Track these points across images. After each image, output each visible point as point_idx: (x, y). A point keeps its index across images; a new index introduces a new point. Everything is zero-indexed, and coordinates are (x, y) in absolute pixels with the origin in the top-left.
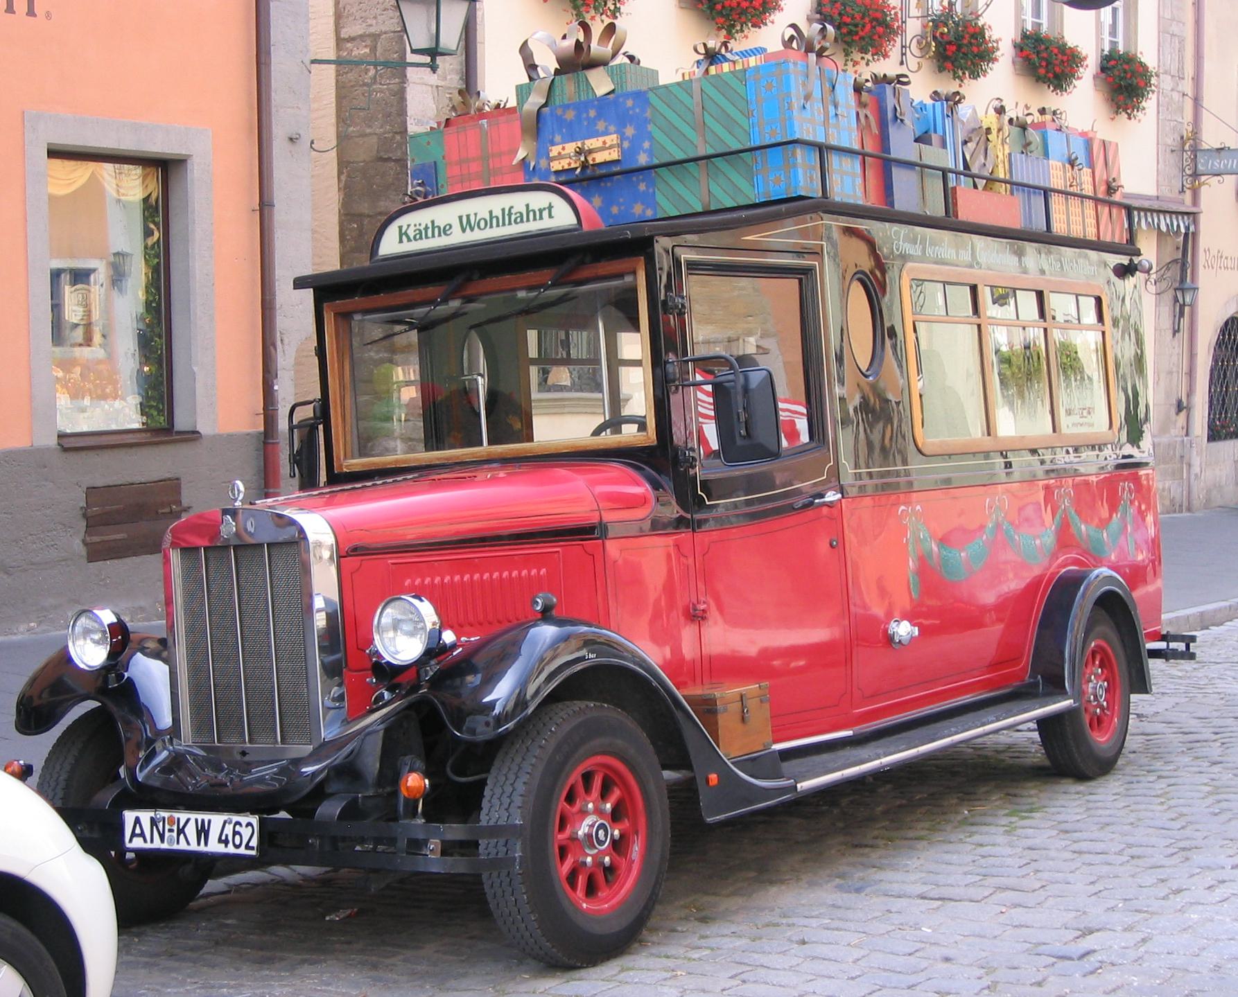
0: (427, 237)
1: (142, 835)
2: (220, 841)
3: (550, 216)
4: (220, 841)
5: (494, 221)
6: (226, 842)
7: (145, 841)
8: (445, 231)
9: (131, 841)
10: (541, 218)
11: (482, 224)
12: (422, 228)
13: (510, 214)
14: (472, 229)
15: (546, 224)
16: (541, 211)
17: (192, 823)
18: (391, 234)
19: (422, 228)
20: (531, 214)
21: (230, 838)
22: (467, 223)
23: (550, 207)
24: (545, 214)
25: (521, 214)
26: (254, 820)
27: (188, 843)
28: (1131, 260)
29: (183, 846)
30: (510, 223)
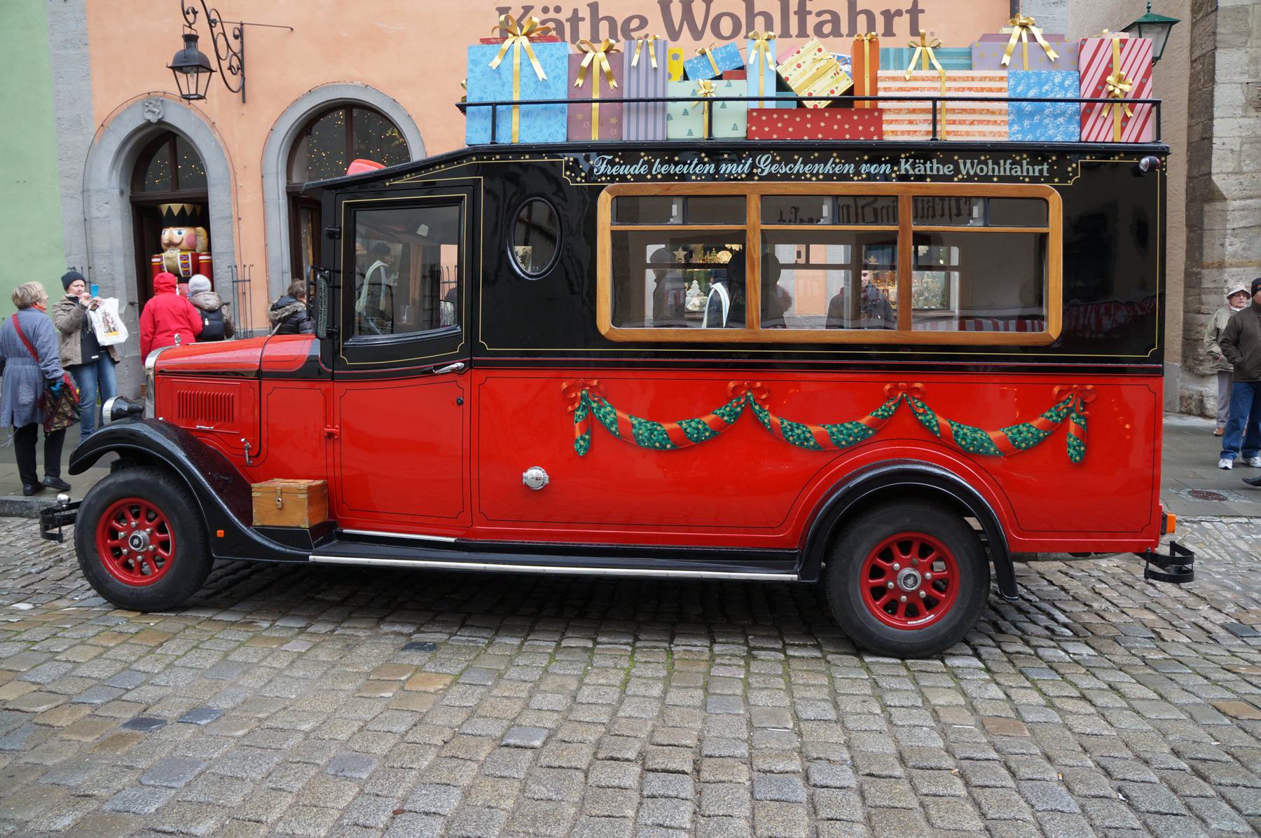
25: (835, 18)
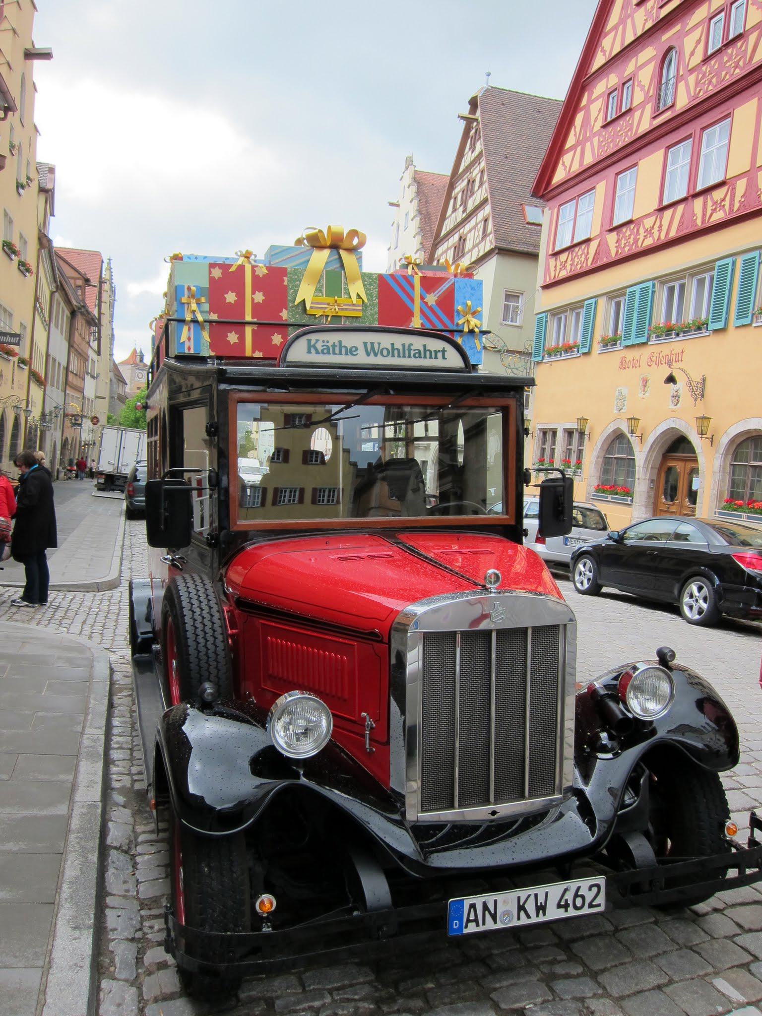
0: (334, 353)
1: (476, 920)
2: (559, 906)
3: (444, 358)
4: (559, 906)
5: (396, 352)
6: (566, 906)
7: (478, 925)
8: (352, 351)
9: (466, 927)
10: (436, 357)
11: (385, 353)
12: (330, 344)
13: (409, 350)
14: (376, 355)
15: (439, 363)
16: (436, 352)
17: (532, 898)
18: (302, 344)
19: (330, 344)
20: (428, 353)
21: (570, 902)
22: (370, 350)
23: (444, 351)
24: (440, 355)
26: (601, 880)
27: (529, 917)
28: (460, 451)
29: (524, 921)
30: (409, 356)
